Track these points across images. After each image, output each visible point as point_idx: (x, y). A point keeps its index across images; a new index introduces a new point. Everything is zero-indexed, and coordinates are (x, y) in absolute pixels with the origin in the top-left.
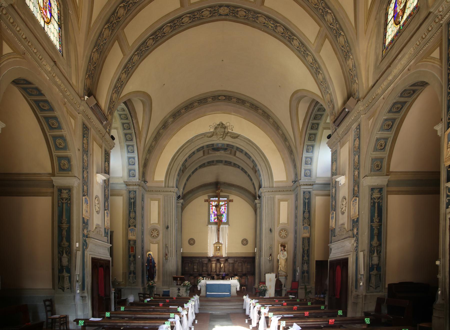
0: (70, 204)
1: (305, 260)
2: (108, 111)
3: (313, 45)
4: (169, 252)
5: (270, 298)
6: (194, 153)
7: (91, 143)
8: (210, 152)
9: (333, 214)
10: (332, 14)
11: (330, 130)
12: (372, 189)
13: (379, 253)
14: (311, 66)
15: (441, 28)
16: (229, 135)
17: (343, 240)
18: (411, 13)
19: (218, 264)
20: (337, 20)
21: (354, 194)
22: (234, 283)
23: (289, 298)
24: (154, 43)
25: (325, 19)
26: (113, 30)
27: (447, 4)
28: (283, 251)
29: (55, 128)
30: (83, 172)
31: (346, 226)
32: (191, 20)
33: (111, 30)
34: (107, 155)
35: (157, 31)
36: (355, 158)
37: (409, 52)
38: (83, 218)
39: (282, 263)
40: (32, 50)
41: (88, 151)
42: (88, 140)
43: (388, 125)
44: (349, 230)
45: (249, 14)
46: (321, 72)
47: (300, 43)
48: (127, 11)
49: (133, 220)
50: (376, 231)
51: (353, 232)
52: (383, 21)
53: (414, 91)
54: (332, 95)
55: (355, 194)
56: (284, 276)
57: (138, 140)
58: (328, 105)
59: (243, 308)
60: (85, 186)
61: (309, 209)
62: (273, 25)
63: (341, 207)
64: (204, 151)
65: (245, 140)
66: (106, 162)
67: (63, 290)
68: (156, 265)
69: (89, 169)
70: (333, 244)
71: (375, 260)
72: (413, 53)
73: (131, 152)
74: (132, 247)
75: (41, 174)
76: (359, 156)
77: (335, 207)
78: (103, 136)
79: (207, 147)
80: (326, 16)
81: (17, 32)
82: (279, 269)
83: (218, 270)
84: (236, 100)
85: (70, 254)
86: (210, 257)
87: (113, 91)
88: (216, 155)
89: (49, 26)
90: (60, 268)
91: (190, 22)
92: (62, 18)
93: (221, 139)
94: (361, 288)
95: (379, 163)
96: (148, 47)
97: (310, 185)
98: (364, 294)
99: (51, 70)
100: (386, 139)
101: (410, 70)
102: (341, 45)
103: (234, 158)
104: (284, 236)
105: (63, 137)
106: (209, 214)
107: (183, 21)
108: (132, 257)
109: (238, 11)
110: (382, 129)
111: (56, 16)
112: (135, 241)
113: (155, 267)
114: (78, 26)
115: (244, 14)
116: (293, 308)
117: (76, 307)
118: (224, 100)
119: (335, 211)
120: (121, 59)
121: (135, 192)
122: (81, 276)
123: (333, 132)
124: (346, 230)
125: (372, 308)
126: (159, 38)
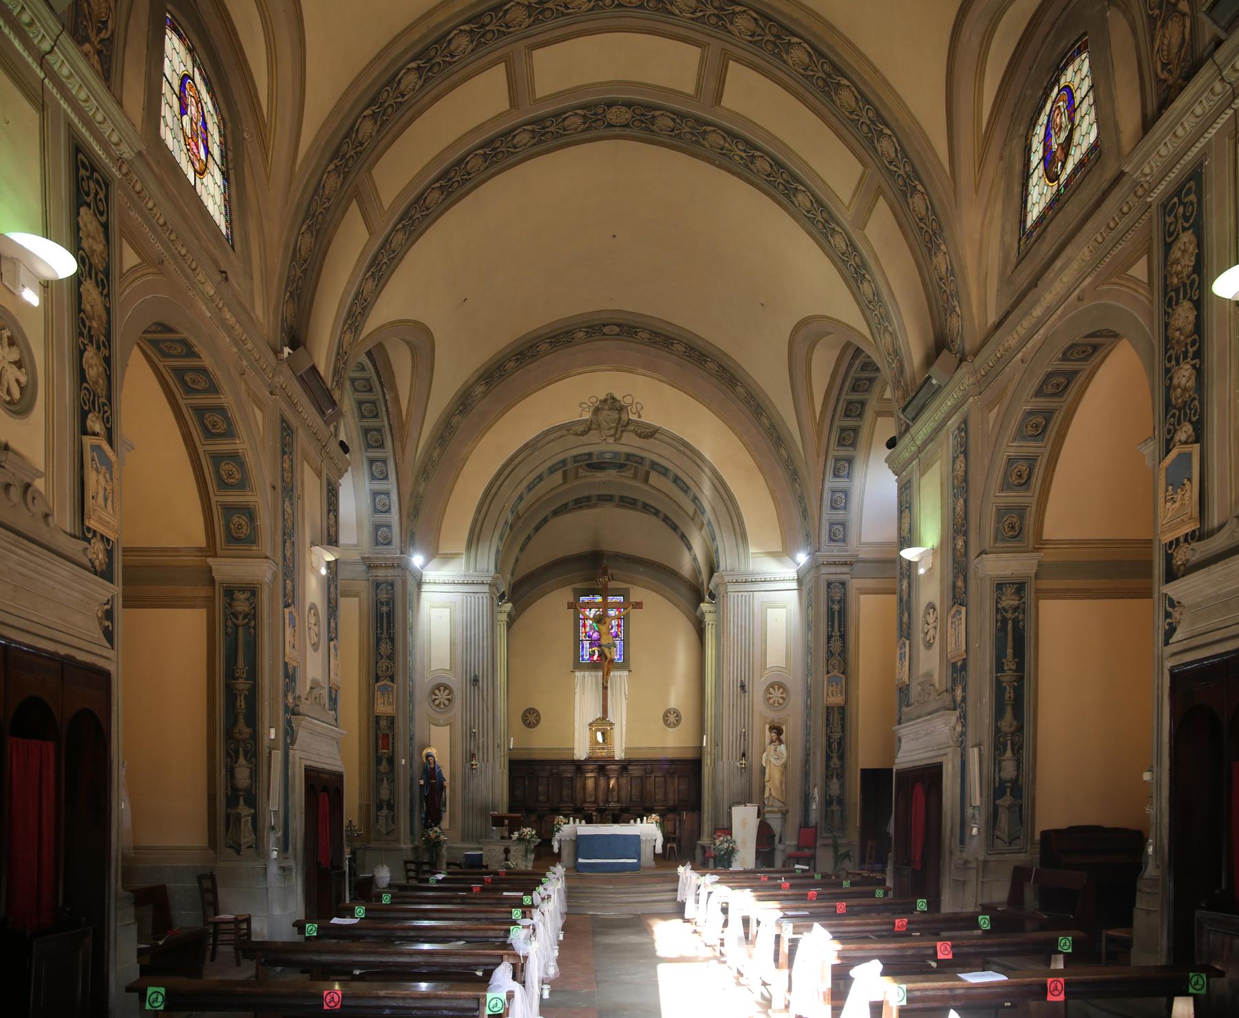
0: (254, 628)
1: (833, 769)
2: (334, 378)
3: (848, 208)
4: (478, 748)
5: (745, 872)
6: (540, 478)
7: (299, 468)
8: (582, 473)
9: (905, 647)
10: (894, 139)
11: (893, 419)
12: (1000, 587)
13: (1018, 749)
14: (844, 261)
15: (1149, 210)
16: (631, 428)
17: (929, 717)
18: (1084, 160)
19: (602, 781)
20: (905, 155)
21: (954, 597)
22: (648, 830)
23: (794, 871)
24: (442, 197)
25: (875, 149)
26: (346, 174)
27: (1161, 159)
28: (777, 743)
29: (220, 435)
30: (285, 543)
31: (936, 676)
32: (536, 140)
33: (342, 176)
34: (333, 495)
35: (451, 168)
36: (956, 505)
37: (1079, 257)
38: (286, 664)
39: (774, 776)
40: (176, 249)
41: (292, 490)
42: (291, 460)
43: (1036, 426)
44: (945, 689)
45: (684, 125)
46: (867, 276)
47: (813, 200)
48: (380, 126)
49: (388, 661)
50: (1009, 694)
51: (953, 696)
52: (1018, 167)
53: (1095, 348)
54: (897, 338)
55: (958, 596)
56: (780, 811)
57: (398, 444)
58: (888, 362)
59: (676, 899)
60: (288, 582)
61: (842, 629)
62: (744, 155)
63: (923, 630)
64: (565, 473)
65: (674, 443)
66: (331, 514)
67: (238, 852)
68: (447, 783)
69: (296, 534)
70: (905, 727)
71: (1009, 771)
72: (1088, 259)
73: (381, 477)
74: (386, 736)
75: (179, 551)
76: (966, 501)
77: (909, 628)
78: (324, 447)
79: (575, 462)
80: (878, 141)
81: (147, 211)
82: (767, 794)
83: (601, 796)
84: (648, 336)
85: (256, 757)
86: (579, 761)
87: (344, 325)
88: (597, 480)
89: (204, 180)
90: (229, 793)
91: (534, 145)
92: (230, 154)
93: (611, 440)
94: (975, 842)
95: (1015, 520)
96: (428, 209)
97: (845, 564)
98: (981, 858)
99: (215, 293)
100: (1032, 461)
101: (1083, 300)
102: (917, 215)
103: (645, 487)
104: (778, 702)
105: (238, 456)
106: (577, 642)
107: (515, 141)
108: (384, 763)
109: (654, 117)
110: (1020, 435)
111: (216, 151)
112: (392, 720)
113: (442, 788)
114: (266, 172)
115: (671, 124)
116: (807, 895)
117: (269, 895)
118: (618, 335)
119: (908, 638)
120: (364, 243)
121: (392, 585)
122: (281, 814)
123: (900, 433)
124: (937, 691)
125: (1000, 894)
126: (456, 185)
